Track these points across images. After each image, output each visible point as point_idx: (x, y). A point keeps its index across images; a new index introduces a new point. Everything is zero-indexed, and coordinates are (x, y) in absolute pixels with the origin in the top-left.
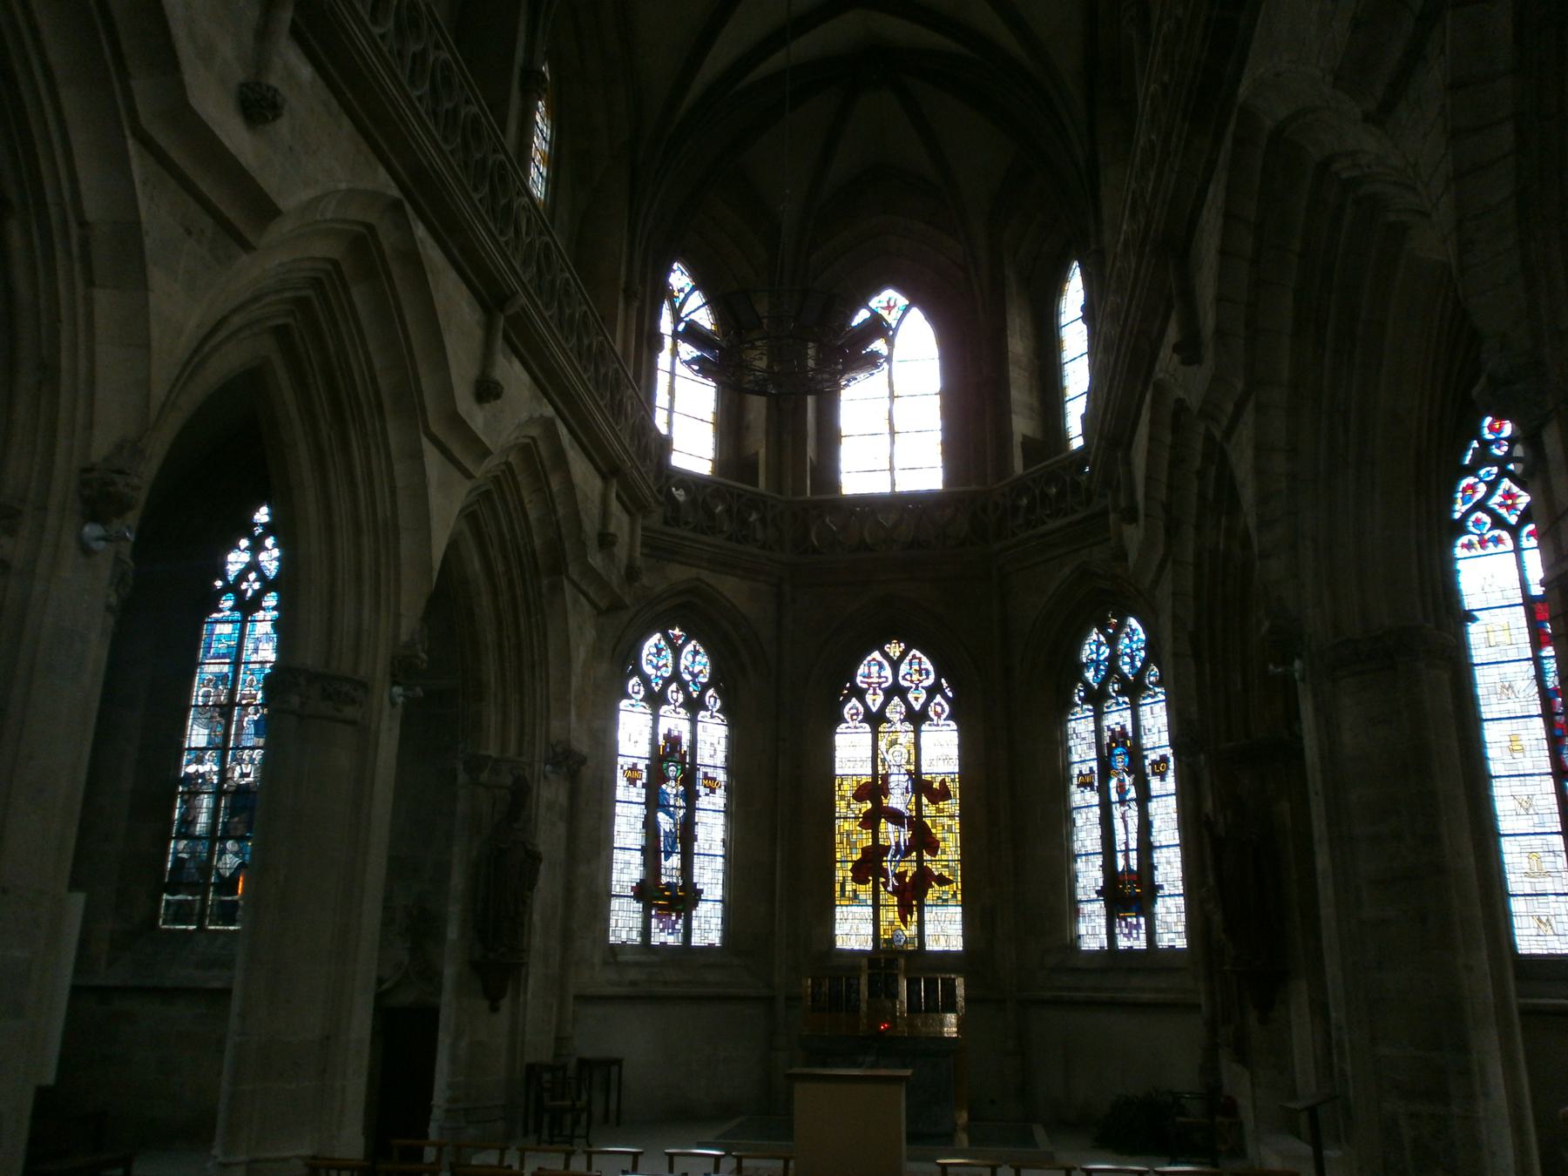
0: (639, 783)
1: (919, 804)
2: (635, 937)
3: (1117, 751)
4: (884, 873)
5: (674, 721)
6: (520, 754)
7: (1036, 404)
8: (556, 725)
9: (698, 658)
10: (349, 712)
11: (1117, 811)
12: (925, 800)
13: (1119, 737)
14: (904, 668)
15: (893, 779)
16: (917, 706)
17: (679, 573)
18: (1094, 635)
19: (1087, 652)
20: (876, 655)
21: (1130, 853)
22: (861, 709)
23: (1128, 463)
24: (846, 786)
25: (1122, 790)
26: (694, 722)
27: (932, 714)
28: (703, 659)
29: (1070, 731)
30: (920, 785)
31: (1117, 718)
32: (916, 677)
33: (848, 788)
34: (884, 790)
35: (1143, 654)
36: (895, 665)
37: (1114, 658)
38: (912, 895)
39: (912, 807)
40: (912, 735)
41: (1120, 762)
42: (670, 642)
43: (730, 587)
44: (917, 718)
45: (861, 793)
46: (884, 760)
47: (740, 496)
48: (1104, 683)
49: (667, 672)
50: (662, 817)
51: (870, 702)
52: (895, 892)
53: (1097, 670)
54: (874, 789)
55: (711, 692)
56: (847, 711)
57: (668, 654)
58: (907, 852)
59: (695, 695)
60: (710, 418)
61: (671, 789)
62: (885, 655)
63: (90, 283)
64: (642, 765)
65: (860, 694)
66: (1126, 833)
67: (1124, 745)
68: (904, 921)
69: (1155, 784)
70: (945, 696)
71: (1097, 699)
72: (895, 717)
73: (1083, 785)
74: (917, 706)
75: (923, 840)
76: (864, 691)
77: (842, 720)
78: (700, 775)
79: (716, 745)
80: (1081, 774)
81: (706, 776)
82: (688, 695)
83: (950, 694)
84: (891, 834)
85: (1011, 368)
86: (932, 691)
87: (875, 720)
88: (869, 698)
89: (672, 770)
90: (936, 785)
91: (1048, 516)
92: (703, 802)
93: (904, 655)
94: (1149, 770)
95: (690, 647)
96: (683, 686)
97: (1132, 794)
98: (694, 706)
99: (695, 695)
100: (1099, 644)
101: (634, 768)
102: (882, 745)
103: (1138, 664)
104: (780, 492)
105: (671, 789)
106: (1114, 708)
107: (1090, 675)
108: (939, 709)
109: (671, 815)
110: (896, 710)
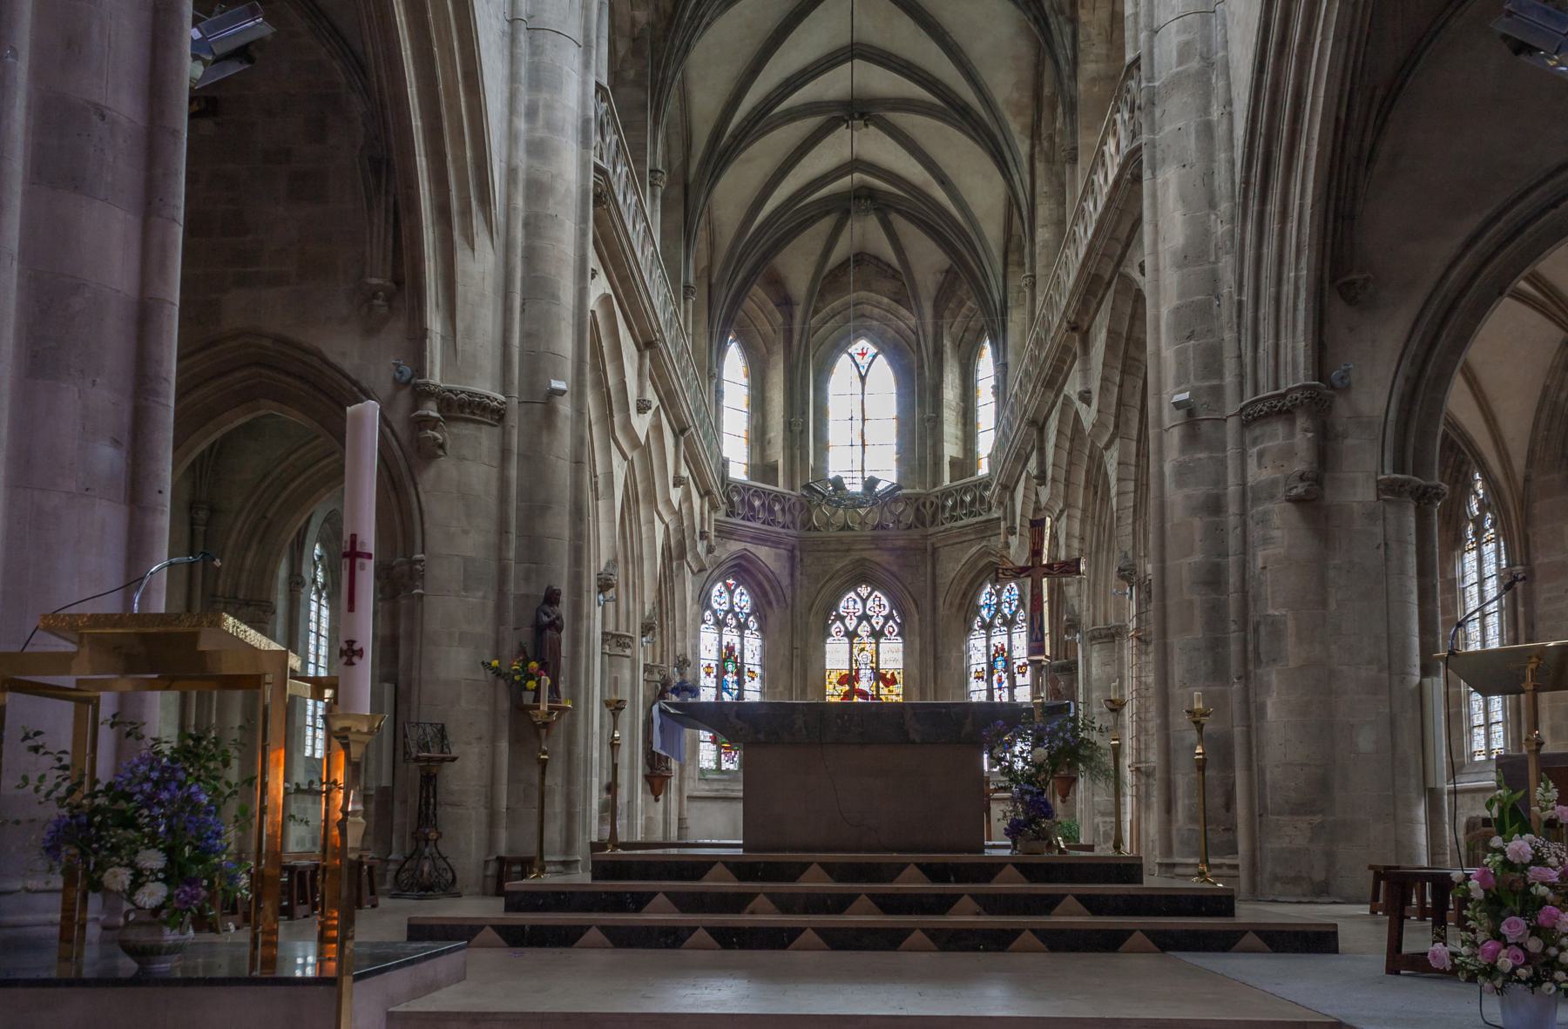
0: (712, 675)
1: (878, 688)
2: (713, 765)
3: (1000, 658)
5: (731, 637)
6: (662, 662)
7: (960, 434)
8: (679, 644)
9: (743, 597)
10: (628, 652)
12: (881, 685)
13: (1000, 651)
14: (870, 603)
15: (862, 672)
17: (735, 547)
18: (988, 588)
19: (983, 599)
20: (852, 594)
21: (1482, 722)
22: (843, 629)
23: (1012, 499)
24: (833, 675)
25: (1000, 681)
26: (742, 637)
27: (886, 632)
28: (746, 598)
29: (971, 646)
30: (879, 676)
31: (999, 639)
32: (877, 609)
33: (834, 678)
34: (857, 679)
35: (1016, 603)
36: (864, 601)
37: (999, 604)
39: (874, 689)
40: (874, 645)
41: (1000, 665)
42: (727, 587)
43: (764, 553)
44: (877, 635)
46: (856, 660)
47: (769, 494)
48: (993, 618)
49: (726, 607)
51: (848, 625)
53: (989, 610)
55: (751, 618)
56: (833, 630)
57: (726, 595)
59: (742, 620)
60: (743, 434)
61: (730, 678)
62: (858, 595)
63: (597, 499)
64: (713, 664)
65: (842, 619)
67: (1003, 655)
69: (1019, 678)
70: (895, 622)
71: (988, 627)
72: (864, 634)
73: (978, 678)
76: (844, 617)
77: (830, 635)
78: (746, 670)
80: (976, 671)
81: (749, 671)
82: (738, 620)
83: (899, 621)
85: (945, 410)
86: (887, 618)
87: (851, 635)
88: (847, 621)
89: (730, 667)
90: (888, 676)
91: (965, 514)
92: (747, 686)
93: (870, 594)
94: (1016, 670)
95: (738, 591)
96: (736, 615)
97: (1006, 684)
98: (742, 627)
99: (742, 620)
100: (991, 595)
101: (709, 666)
102: (855, 651)
103: (1014, 608)
104: (792, 490)
105: (730, 678)
106: (998, 633)
107: (984, 612)
108: (891, 630)
109: (730, 694)
110: (864, 629)
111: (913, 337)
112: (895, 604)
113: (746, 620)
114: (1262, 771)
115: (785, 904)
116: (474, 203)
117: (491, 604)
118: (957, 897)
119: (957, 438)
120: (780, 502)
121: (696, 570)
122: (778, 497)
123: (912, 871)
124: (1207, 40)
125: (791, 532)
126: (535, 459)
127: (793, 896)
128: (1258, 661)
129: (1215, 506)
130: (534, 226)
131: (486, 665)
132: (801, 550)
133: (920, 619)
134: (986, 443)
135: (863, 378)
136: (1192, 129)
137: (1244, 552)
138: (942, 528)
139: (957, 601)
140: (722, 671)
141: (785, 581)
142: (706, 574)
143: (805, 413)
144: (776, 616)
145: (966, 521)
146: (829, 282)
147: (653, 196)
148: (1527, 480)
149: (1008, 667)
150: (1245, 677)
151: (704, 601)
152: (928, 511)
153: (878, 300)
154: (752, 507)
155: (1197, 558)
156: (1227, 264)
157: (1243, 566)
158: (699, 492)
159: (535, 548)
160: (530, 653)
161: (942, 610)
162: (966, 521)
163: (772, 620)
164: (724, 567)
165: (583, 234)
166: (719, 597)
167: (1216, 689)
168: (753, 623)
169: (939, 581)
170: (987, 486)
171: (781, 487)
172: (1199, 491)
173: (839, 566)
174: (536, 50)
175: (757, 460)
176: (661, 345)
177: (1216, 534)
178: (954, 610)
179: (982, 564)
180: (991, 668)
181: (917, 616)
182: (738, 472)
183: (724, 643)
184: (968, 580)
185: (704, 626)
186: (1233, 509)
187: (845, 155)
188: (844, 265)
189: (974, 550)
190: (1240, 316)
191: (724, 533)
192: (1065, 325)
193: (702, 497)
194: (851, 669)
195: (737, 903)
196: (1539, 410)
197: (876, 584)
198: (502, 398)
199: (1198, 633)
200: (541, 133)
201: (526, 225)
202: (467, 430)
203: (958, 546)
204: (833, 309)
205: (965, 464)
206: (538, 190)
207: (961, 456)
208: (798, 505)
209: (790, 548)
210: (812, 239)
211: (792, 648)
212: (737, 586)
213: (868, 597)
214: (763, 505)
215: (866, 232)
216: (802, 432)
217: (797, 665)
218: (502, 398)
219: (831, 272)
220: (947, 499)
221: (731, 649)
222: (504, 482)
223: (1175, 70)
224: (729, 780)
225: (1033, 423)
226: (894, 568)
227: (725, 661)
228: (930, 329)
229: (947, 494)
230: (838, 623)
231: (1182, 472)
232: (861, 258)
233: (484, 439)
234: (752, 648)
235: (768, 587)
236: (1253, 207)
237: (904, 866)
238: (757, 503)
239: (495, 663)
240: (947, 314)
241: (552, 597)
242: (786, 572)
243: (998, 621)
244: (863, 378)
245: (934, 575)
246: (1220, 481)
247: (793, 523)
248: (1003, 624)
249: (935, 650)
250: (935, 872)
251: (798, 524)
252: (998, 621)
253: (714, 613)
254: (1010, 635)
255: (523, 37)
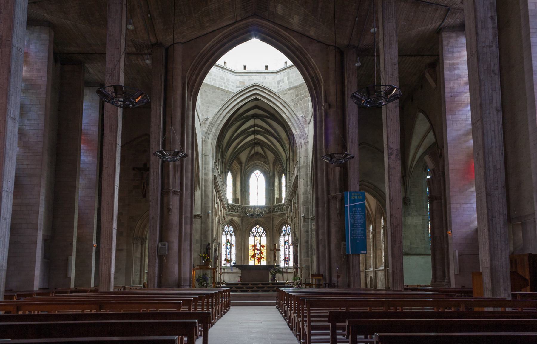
1: (261, 248)
4: (256, 257)
7: (278, 192)
8: (218, 240)
11: (286, 250)
13: (287, 241)
14: (259, 229)
16: (261, 235)
17: (230, 218)
18: (284, 227)
20: (255, 227)
25: (287, 247)
26: (231, 237)
28: (232, 228)
30: (261, 246)
32: (260, 231)
34: (256, 246)
36: (258, 229)
38: (259, 260)
41: (287, 243)
42: (228, 226)
43: (236, 219)
44: (260, 236)
45: (253, 246)
48: (285, 233)
49: (228, 231)
50: (227, 250)
52: (257, 259)
54: (254, 246)
55: (233, 233)
56: (251, 235)
57: (228, 228)
58: (259, 254)
61: (228, 246)
62: (256, 227)
64: (225, 244)
66: (287, 253)
68: (258, 263)
69: (290, 246)
71: (284, 235)
74: (261, 235)
75: (261, 253)
77: (250, 236)
79: (301, 279)
82: (230, 233)
84: (257, 252)
86: (263, 233)
87: (255, 236)
88: (254, 233)
89: (229, 244)
90: (263, 245)
93: (259, 227)
95: (230, 227)
96: (230, 232)
98: (231, 235)
100: (285, 228)
101: (224, 244)
102: (256, 240)
103: (289, 232)
104: (242, 204)
107: (283, 232)
110: (258, 235)
111: (268, 171)
112: (264, 229)
113: (232, 233)
114: (313, 270)
115: (247, 288)
116: (197, 185)
117: (200, 246)
118: (265, 287)
119: (278, 193)
120: (239, 207)
121: (221, 224)
122: (239, 207)
123: (260, 284)
124: (307, 162)
125: (242, 214)
126: (206, 223)
127: (248, 287)
128: (313, 255)
129: (307, 231)
130: (206, 186)
131: (200, 255)
132: (244, 218)
133: (270, 233)
134: (284, 195)
135: (257, 179)
136: (305, 174)
137: (311, 238)
138: (274, 214)
139: (278, 230)
140: (227, 245)
141: (240, 225)
142: (223, 224)
143: (245, 187)
144: (238, 232)
145: (279, 213)
146: (250, 158)
147: (219, 164)
148: (375, 216)
149: (288, 244)
150: (311, 257)
151: (223, 230)
152: (271, 210)
153: (260, 163)
154: (233, 209)
155: (305, 239)
156: (309, 195)
157: (311, 241)
158: (216, 191)
159: (206, 237)
160: (205, 253)
161: (275, 231)
162: (279, 213)
163: (237, 233)
164: (227, 222)
165: (213, 187)
166: (226, 229)
167: (307, 258)
168: (233, 234)
169: (274, 225)
170: (284, 206)
171: (239, 204)
172: (305, 229)
173: (252, 221)
174: (206, 159)
175: (234, 198)
176: (220, 191)
177: (308, 235)
178: (277, 231)
179: (283, 222)
180: (285, 244)
181: (319, 89)
182: (230, 202)
183: (227, 239)
184: (280, 225)
185: (223, 235)
186: (310, 232)
187: (253, 123)
188: (253, 155)
189: (281, 219)
190: (311, 204)
191: (227, 215)
192: (292, 190)
193: (223, 209)
194: (255, 244)
195: (242, 288)
196: (376, 205)
197: (260, 225)
198: (201, 214)
199: (305, 250)
200: (206, 172)
201: (204, 186)
202: (196, 219)
203: (278, 218)
204: (251, 164)
205: (279, 199)
206: (206, 181)
207: (278, 197)
208: (243, 208)
209: (241, 217)
210: (246, 152)
211: (242, 239)
212: (230, 226)
213: (258, 228)
214: (236, 208)
215: (258, 149)
216: (244, 191)
217: (243, 243)
218: (201, 214)
219: (251, 156)
220: (275, 207)
221: (229, 240)
222: (201, 227)
223: (303, 165)
224: (228, 269)
225: (289, 200)
226: (264, 222)
227: (227, 242)
228: (272, 170)
229: (275, 206)
230: (252, 234)
231: (303, 226)
232: (257, 153)
233: (199, 220)
234: (233, 239)
235: (236, 226)
236: (312, 189)
237: (259, 284)
238: (234, 208)
239: (201, 255)
240: (275, 166)
241: (209, 244)
242: (241, 222)
243: (286, 234)
244: (257, 179)
245: (273, 224)
246: (308, 228)
247: (242, 212)
248: (287, 235)
249: (273, 240)
250: (263, 284)
251: (243, 212)
252: (286, 234)
253: (225, 232)
254: (288, 237)
255: (204, 157)
